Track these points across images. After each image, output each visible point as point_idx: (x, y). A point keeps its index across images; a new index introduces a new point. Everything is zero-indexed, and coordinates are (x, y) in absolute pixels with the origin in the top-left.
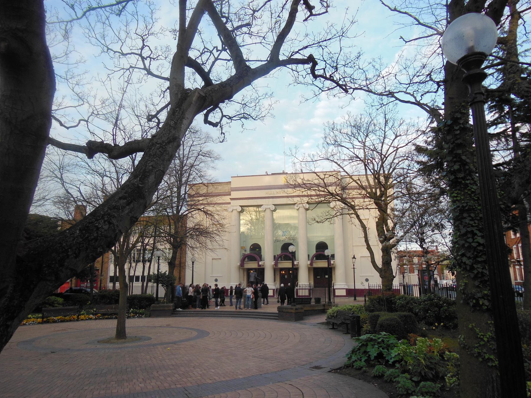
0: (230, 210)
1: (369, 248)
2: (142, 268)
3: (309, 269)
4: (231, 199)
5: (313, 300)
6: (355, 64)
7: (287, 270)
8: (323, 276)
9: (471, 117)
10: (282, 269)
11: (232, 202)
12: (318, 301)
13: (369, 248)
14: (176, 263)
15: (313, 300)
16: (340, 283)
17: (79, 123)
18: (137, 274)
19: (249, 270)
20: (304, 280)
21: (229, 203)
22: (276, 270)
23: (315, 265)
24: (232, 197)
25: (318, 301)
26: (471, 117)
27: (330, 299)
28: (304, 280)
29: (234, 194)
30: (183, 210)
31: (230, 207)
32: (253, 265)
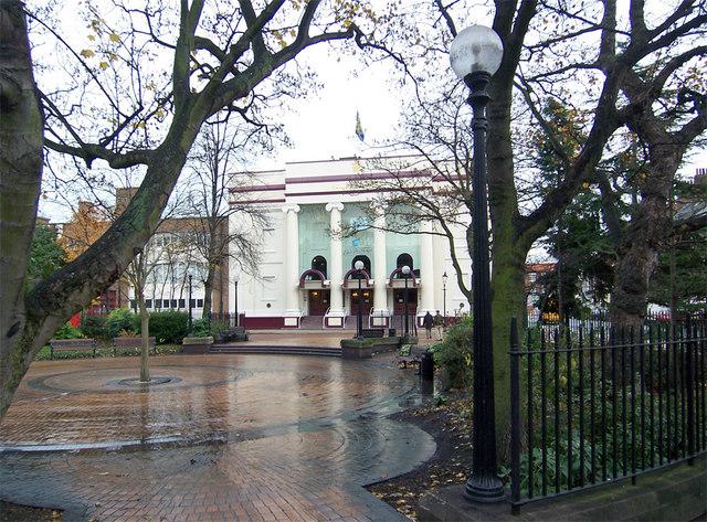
0: (285, 210)
1: (456, 265)
2: (165, 281)
3: (388, 291)
4: (287, 195)
5: (386, 331)
6: (435, 62)
7: (361, 291)
8: (406, 298)
9: (489, 221)
10: (353, 291)
11: (287, 198)
12: (392, 333)
13: (456, 265)
14: (217, 282)
15: (386, 331)
16: (428, 305)
17: (73, 110)
18: (165, 298)
19: (311, 291)
20: (382, 306)
21: (287, 195)
22: (388, 291)
23: (395, 286)
24: (287, 191)
25: (392, 333)
26: (489, 221)
27: (407, 331)
28: (382, 306)
29: (291, 189)
30: (223, 207)
31: (284, 207)
32: (316, 285)
